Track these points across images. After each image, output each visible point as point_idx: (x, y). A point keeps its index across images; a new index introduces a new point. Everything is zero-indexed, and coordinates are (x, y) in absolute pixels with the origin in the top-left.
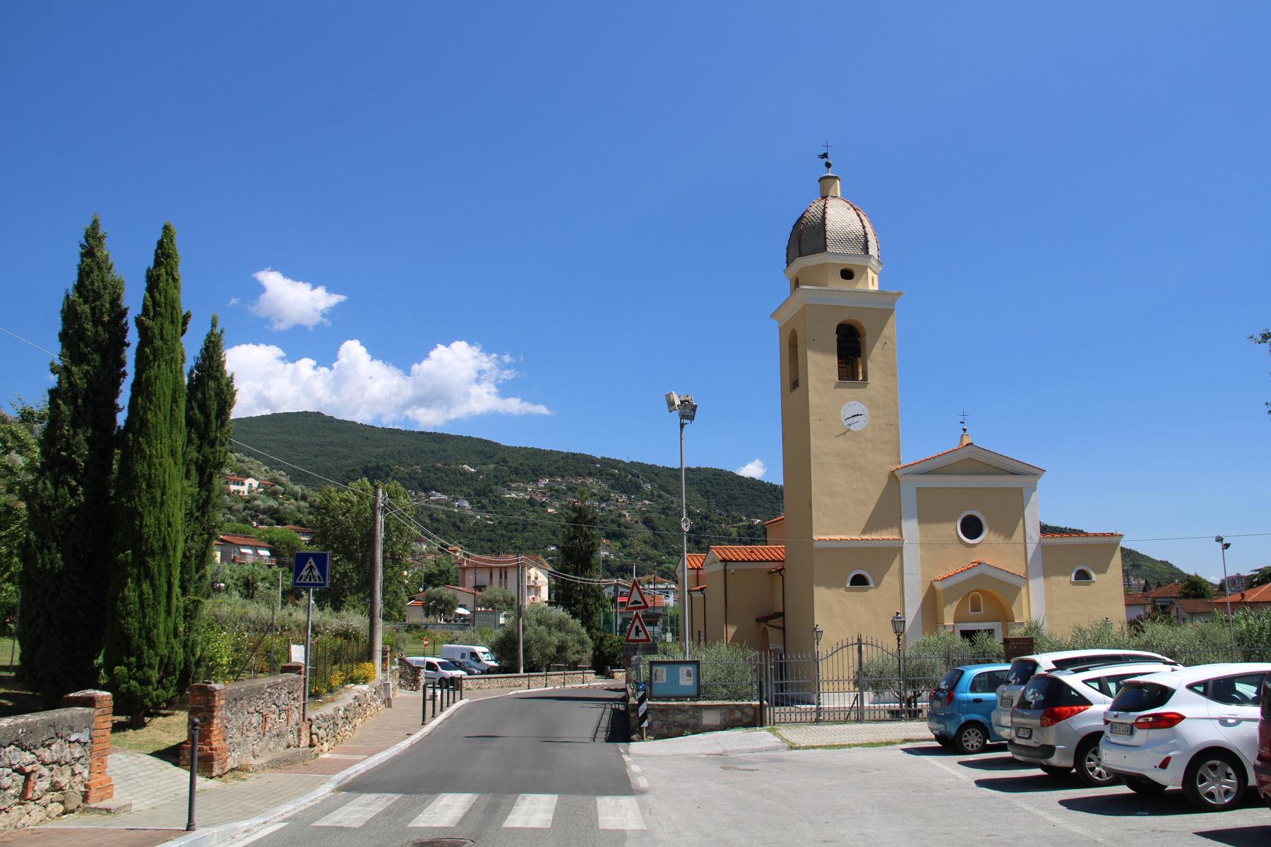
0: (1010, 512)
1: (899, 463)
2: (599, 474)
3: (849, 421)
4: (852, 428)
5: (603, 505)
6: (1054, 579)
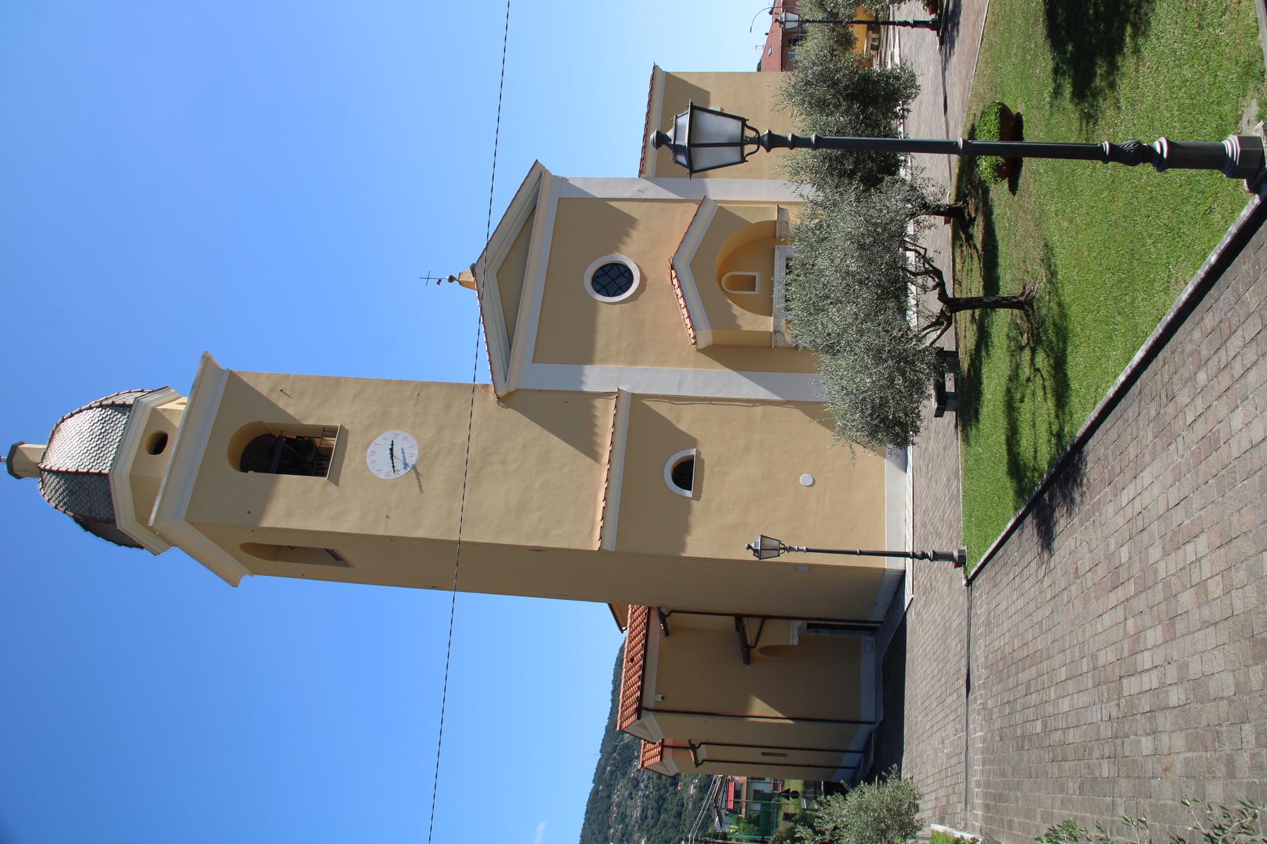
1: (485, 386)
2: (610, 787)
3: (399, 465)
4: (411, 461)
5: (642, 786)
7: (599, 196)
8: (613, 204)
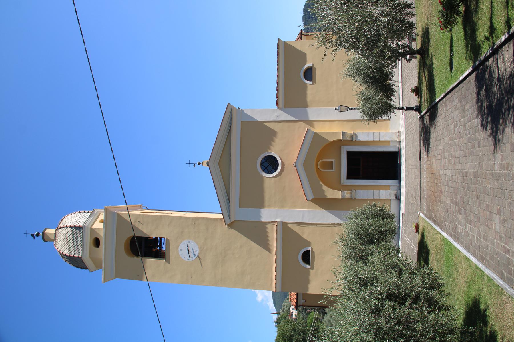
0: (258, 132)
3: (192, 255)
4: (197, 253)
6: (309, 98)
7: (259, 119)
8: (266, 124)
